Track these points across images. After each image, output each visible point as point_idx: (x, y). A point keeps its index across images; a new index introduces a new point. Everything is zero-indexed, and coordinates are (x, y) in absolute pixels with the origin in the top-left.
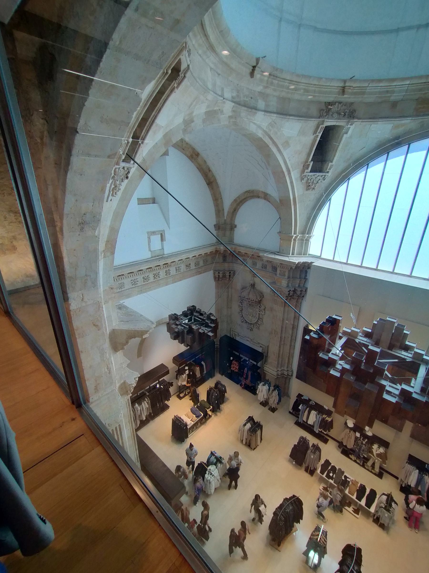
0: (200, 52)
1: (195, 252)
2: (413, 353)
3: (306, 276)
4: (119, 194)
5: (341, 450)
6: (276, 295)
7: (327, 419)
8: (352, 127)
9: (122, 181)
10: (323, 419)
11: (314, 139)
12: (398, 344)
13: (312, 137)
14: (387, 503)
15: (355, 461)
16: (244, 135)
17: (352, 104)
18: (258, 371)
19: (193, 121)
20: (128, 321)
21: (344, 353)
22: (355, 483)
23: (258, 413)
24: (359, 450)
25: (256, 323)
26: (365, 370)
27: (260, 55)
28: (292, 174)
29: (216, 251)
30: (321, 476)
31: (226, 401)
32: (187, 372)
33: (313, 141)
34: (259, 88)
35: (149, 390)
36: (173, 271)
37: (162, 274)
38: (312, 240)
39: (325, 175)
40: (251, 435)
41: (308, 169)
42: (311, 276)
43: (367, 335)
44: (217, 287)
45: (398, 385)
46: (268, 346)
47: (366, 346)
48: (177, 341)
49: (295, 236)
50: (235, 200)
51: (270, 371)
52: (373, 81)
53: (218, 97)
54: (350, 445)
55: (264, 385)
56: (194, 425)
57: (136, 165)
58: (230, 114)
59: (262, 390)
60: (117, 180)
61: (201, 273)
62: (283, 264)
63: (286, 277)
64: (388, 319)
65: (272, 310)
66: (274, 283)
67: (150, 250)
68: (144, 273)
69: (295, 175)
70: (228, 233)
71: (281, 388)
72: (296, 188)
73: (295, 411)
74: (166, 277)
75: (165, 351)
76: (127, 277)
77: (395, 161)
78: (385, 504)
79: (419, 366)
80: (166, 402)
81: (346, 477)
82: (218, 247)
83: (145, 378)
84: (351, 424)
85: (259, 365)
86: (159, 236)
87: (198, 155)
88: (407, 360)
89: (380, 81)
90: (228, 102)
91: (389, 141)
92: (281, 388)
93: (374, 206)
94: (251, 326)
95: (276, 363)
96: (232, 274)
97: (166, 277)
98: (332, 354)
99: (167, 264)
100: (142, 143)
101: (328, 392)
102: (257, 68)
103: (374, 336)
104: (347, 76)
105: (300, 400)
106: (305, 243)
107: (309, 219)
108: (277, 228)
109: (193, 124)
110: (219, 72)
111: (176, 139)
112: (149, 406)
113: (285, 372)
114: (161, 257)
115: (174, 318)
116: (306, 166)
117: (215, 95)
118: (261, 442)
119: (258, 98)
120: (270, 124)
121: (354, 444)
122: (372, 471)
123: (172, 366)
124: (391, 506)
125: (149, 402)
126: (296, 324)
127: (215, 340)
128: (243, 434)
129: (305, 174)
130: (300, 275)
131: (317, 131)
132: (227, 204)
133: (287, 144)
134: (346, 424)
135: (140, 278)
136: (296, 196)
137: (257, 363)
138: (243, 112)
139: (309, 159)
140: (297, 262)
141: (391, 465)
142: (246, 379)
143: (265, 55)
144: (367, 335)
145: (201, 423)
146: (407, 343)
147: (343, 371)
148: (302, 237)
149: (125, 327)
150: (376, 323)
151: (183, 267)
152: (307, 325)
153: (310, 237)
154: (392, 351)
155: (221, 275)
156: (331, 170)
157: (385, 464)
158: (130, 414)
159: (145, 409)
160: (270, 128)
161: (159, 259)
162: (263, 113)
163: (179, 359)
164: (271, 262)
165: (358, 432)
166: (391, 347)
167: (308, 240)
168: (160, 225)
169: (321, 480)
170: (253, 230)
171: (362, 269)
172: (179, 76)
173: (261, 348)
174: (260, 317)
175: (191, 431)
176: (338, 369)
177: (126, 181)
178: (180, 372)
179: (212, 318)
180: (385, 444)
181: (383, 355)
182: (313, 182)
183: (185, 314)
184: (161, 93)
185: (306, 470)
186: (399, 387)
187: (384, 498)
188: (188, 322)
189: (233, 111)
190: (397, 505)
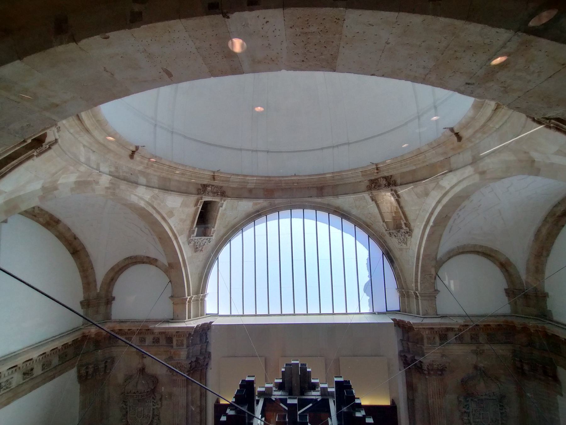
2: (319, 389)
3: (207, 338)
6: (175, 374)
8: (225, 203)
12: (306, 386)
13: (194, 209)
16: (125, 205)
17: (221, 187)
19: (56, 189)
28: (179, 239)
34: (140, 168)
38: (207, 299)
41: (193, 233)
42: (213, 337)
43: (280, 387)
47: (284, 401)
49: (189, 297)
50: (113, 269)
52: (233, 175)
58: (107, 185)
62: (180, 332)
63: (185, 346)
64: (292, 362)
65: (171, 395)
69: (182, 239)
70: (102, 309)
79: (328, 400)
82: (86, 331)
87: (58, 222)
88: (318, 400)
89: (238, 175)
104: (216, 169)
106: (201, 302)
107: (200, 278)
109: (55, 192)
110: (94, 149)
116: (191, 232)
117: (88, 167)
120: (153, 197)
132: (101, 273)
133: (171, 213)
136: (186, 258)
138: (123, 186)
140: (195, 326)
144: (280, 387)
146: (313, 381)
150: (283, 370)
153: (205, 296)
155: (91, 371)
160: (153, 200)
164: (164, 333)
167: (203, 300)
170: (137, 300)
171: (257, 317)
174: (156, 413)
181: (303, 403)
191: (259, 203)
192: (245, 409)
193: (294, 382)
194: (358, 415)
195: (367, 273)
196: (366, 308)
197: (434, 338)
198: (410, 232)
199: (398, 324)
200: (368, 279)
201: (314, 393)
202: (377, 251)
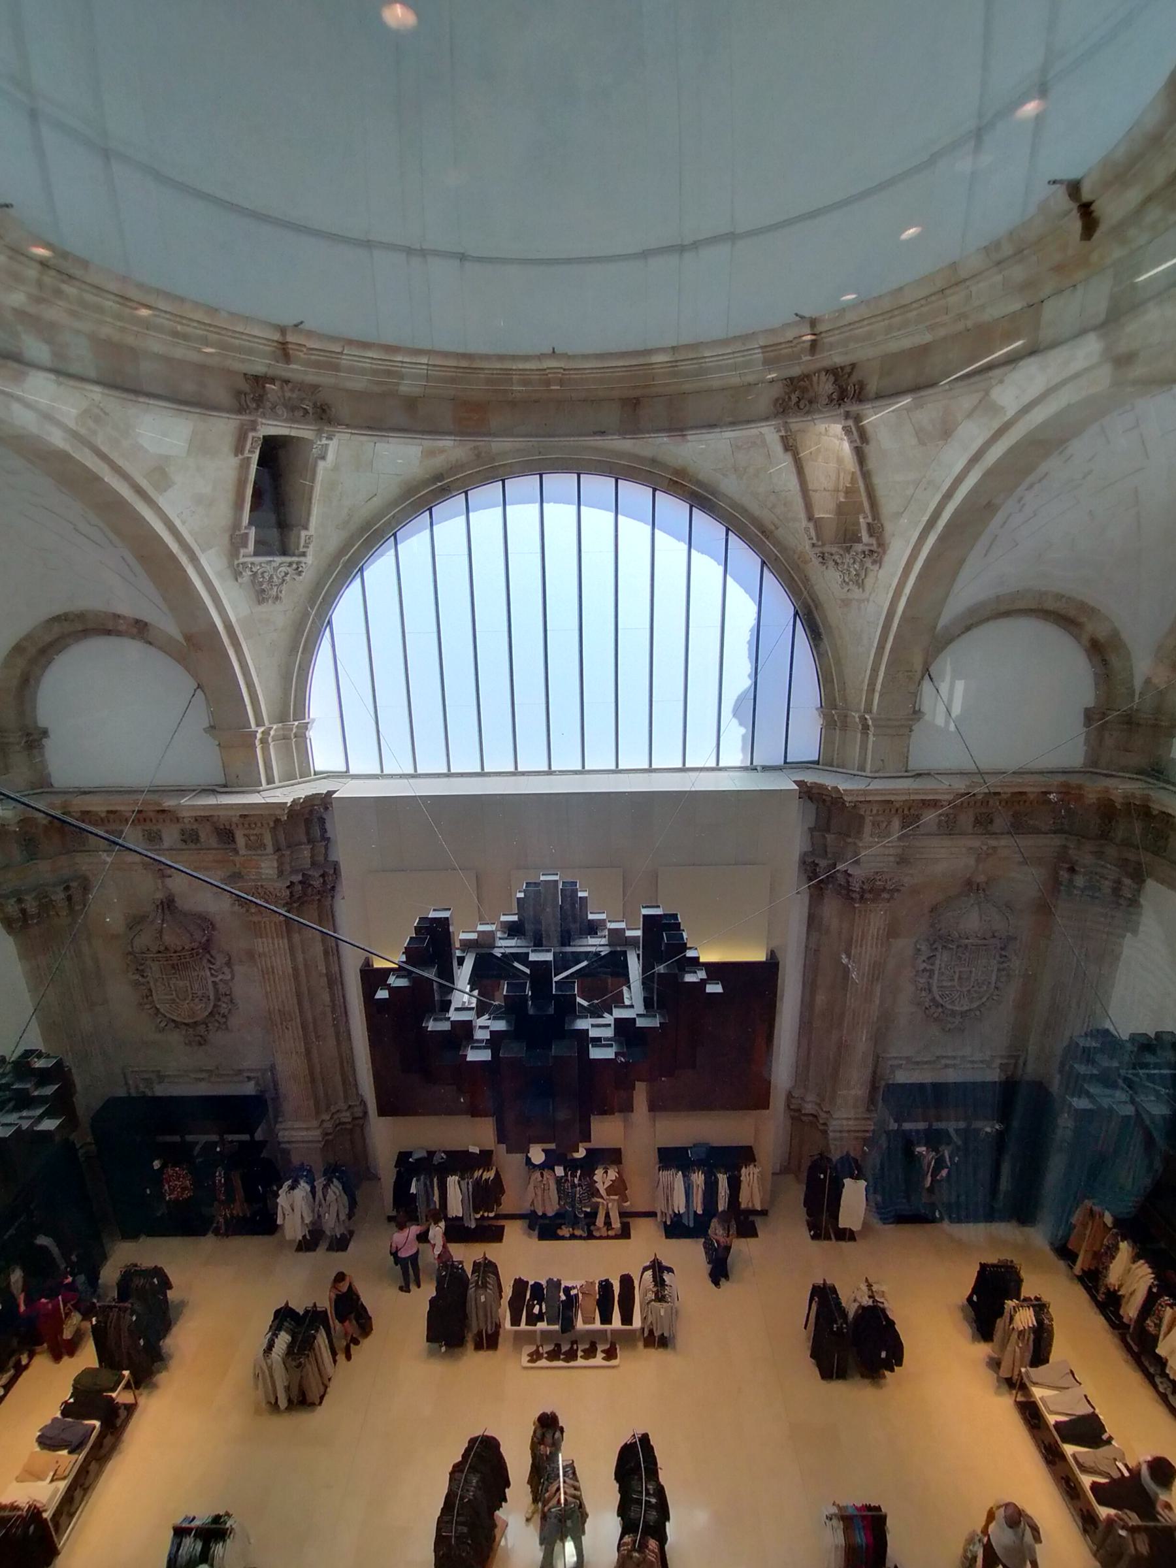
7: (486, 1175)
8: (333, 445)
10: (477, 1183)
11: (241, 466)
13: (234, 461)
15: (573, 1237)
17: (315, 388)
18: (264, 1155)
24: (573, 1207)
25: (211, 1013)
26: (539, 1011)
30: (516, 1332)
39: (298, 563)
40: (299, 1365)
41: (245, 546)
42: (339, 827)
43: (513, 930)
44: (26, 952)
45: (606, 1015)
46: (273, 1068)
47: (523, 958)
49: (261, 730)
50: (18, 649)
52: (350, 342)
54: (551, 1206)
55: (292, 1188)
59: (294, 1205)
62: (248, 816)
63: (270, 849)
65: (251, 955)
66: (235, 877)
69: (212, 562)
71: (346, 1168)
72: (227, 600)
77: (449, 527)
79: (625, 954)
81: (567, 1290)
84: (537, 1155)
85: (259, 1135)
89: (366, 345)
92: (346, 1168)
94: (196, 1033)
95: (312, 1102)
96: (77, 890)
98: (457, 1009)
103: (528, 927)
104: (288, 320)
105: (407, 1166)
106: (296, 743)
107: (286, 677)
108: (200, 717)
116: (236, 543)
118: (335, 1361)
121: (560, 1198)
122: (611, 1233)
127: (72, 1137)
128: (272, 1376)
129: (242, 560)
130: (308, 833)
134: (528, 1160)
136: (233, 620)
137: (252, 1136)
140: (289, 800)
143: (8, 202)
144: (513, 930)
146: (591, 917)
147: (496, 1040)
150: (521, 895)
153: (306, 726)
155: (31, 906)
156: (311, 546)
164: (207, 818)
165: (559, 1165)
166: (566, 940)
167: (302, 736)
169: (520, 1339)
173: (252, 1083)
179: (39, 1064)
180: (613, 1156)
181: (563, 962)
186: (608, 1019)
187: (649, 1274)
192: (430, 974)
194: (689, 978)
195: (747, 667)
196: (733, 755)
197: (889, 823)
198: (876, 554)
199: (808, 793)
200: (748, 683)
202: (781, 606)
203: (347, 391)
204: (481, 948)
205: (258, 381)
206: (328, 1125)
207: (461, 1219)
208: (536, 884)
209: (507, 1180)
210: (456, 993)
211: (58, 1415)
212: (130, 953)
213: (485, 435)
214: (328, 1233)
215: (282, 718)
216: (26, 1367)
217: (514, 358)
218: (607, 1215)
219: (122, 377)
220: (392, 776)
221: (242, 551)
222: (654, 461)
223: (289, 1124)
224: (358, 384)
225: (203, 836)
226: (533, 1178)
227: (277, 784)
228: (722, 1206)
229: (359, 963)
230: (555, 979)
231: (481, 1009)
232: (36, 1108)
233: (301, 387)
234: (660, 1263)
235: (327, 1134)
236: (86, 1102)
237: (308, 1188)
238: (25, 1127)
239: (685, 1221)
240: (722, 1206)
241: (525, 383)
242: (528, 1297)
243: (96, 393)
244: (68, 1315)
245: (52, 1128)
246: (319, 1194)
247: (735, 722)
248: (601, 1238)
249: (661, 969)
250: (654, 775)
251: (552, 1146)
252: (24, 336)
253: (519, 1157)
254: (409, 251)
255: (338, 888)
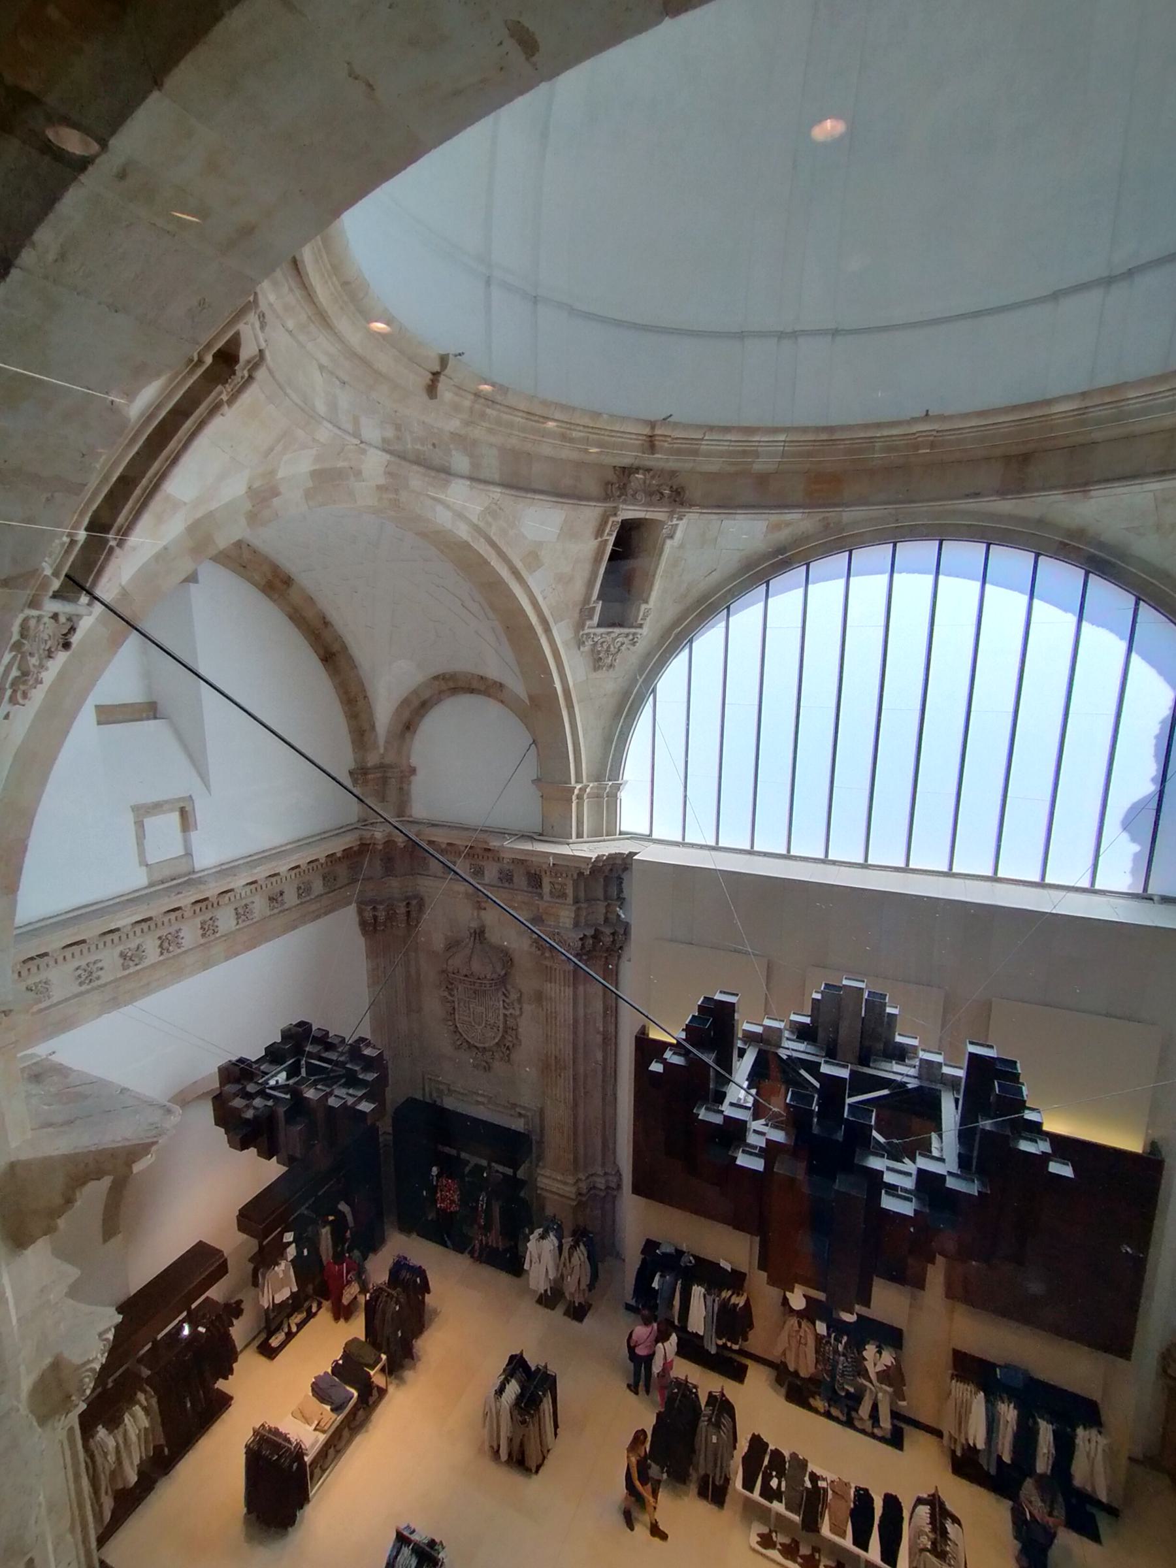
0: (290, 324)
1: (295, 857)
3: (621, 891)
4: (38, 695)
5: (783, 1391)
7: (734, 1300)
8: (682, 525)
9: (50, 657)
10: (724, 1305)
11: (599, 547)
12: (881, 1046)
13: (593, 544)
14: (934, 1530)
15: (828, 1415)
16: (423, 535)
17: (673, 473)
18: (522, 1194)
20: (70, 1122)
21: (757, 1094)
22: (840, 1488)
23: (534, 1335)
26: (828, 1137)
27: (452, 350)
29: (362, 845)
31: (431, 1321)
32: (291, 1252)
33: (597, 554)
35: (151, 1359)
36: (226, 920)
37: (190, 934)
38: (624, 796)
39: (634, 634)
40: (524, 1422)
41: (591, 618)
43: (803, 1033)
45: (906, 1160)
46: (542, 1111)
47: (813, 1068)
48: (253, 1151)
49: (579, 786)
50: (405, 702)
51: (555, 1186)
52: (711, 428)
53: (348, 437)
54: (806, 1365)
55: (543, 1237)
56: (327, 1445)
57: (98, 608)
58: (382, 481)
59: (541, 1252)
60: (31, 655)
61: (318, 917)
62: (563, 866)
63: (570, 900)
64: (845, 982)
65: (539, 997)
66: (538, 920)
67: (143, 862)
68: (124, 937)
69: (562, 633)
71: (591, 1236)
72: (572, 669)
73: (645, 1302)
74: (202, 941)
75: (206, 1192)
76: (60, 959)
77: (784, 600)
78: (932, 1536)
80: (221, 1384)
81: (814, 1478)
82: (367, 835)
83: (140, 1310)
84: (797, 1301)
85: (521, 1174)
86: (175, 817)
87: (288, 581)
88: (910, 1086)
89: (726, 429)
90: (372, 451)
91: (765, 557)
92: (591, 1236)
93: (685, 700)
96: (415, 906)
97: (202, 941)
98: (732, 1104)
99: (206, 899)
100: (120, 544)
101: (738, 1223)
102: (442, 378)
103: (821, 1035)
105: (655, 1258)
106: (607, 803)
107: (608, 740)
108: (530, 770)
109: (276, 501)
110: (346, 379)
111: (223, 541)
112: (152, 1421)
113: (598, 1180)
114: (188, 879)
115: (238, 1073)
116: (585, 613)
118: (556, 1434)
119: (452, 446)
121: (817, 1362)
122: (876, 1431)
123: (233, 1243)
124: (944, 1533)
125: (154, 1401)
126: (612, 1029)
129: (586, 631)
130: (606, 892)
131: (603, 531)
132: (384, 712)
134: (785, 1301)
135: (109, 957)
137: (516, 1170)
138: (416, 479)
139: (591, 594)
140: (594, 856)
141: (921, 1399)
142: (487, 1228)
144: (803, 1033)
145: (350, 1429)
146: (898, 1039)
147: (770, 1151)
148: (597, 788)
149: (61, 1145)
150: (819, 996)
151: (259, 905)
152: (644, 1027)
153: (618, 787)
154: (869, 1066)
157: (904, 1400)
158: (79, 1492)
159: (134, 1438)
161: (178, 889)
162: (468, 483)
163: (258, 1217)
164: (522, 862)
165: (821, 1320)
166: (864, 1060)
167: (613, 798)
168: (177, 780)
169: (751, 1512)
170: (463, 776)
172: (234, 374)
175: (317, 1471)
176: (755, 1147)
177: (62, 656)
178: (264, 1259)
179: (367, 1052)
180: (891, 1337)
181: (861, 1083)
182: (608, 650)
183: (273, 1055)
184: (180, 413)
185: (703, 1494)
186: (908, 1166)
187: (924, 1511)
188: (288, 1078)
189: (389, 474)
190: (960, 1524)
191: (788, 524)
192: (709, 1059)
193: (843, 1032)
194: (1025, 1146)
195: (1152, 768)
200: (1150, 788)
201: (897, 1068)
203: (701, 473)
204: (765, 1042)
205: (626, 472)
206: (583, 1186)
207: (702, 1338)
208: (840, 988)
209: (756, 1311)
210: (732, 1086)
211: (329, 1371)
212: (443, 971)
213: (835, 505)
214: (567, 1295)
215: (598, 778)
216: (315, 1314)
217: (878, 425)
218: (875, 1407)
219: (518, 481)
220: (693, 845)
221: (588, 623)
222: (1041, 522)
223: (548, 1173)
224: (713, 466)
225: (515, 879)
226: (787, 1327)
227: (586, 839)
228: (1042, 1465)
229: (636, 1030)
230: (849, 1101)
231: (758, 1111)
232: (359, 1090)
233: (661, 473)
234: (942, 1504)
235: (580, 1194)
236: (395, 1095)
237: (556, 1243)
238: (349, 1103)
239: (983, 1461)
240: (1042, 1465)
241: (890, 449)
242: (766, 1462)
243: (496, 492)
244: (349, 1282)
245: (368, 1111)
246: (565, 1253)
247: (1125, 836)
248: (863, 1432)
249: (987, 1124)
250: (998, 885)
251: (821, 1296)
252: (454, 452)
253: (774, 1293)
254: (781, 335)
255: (625, 949)
